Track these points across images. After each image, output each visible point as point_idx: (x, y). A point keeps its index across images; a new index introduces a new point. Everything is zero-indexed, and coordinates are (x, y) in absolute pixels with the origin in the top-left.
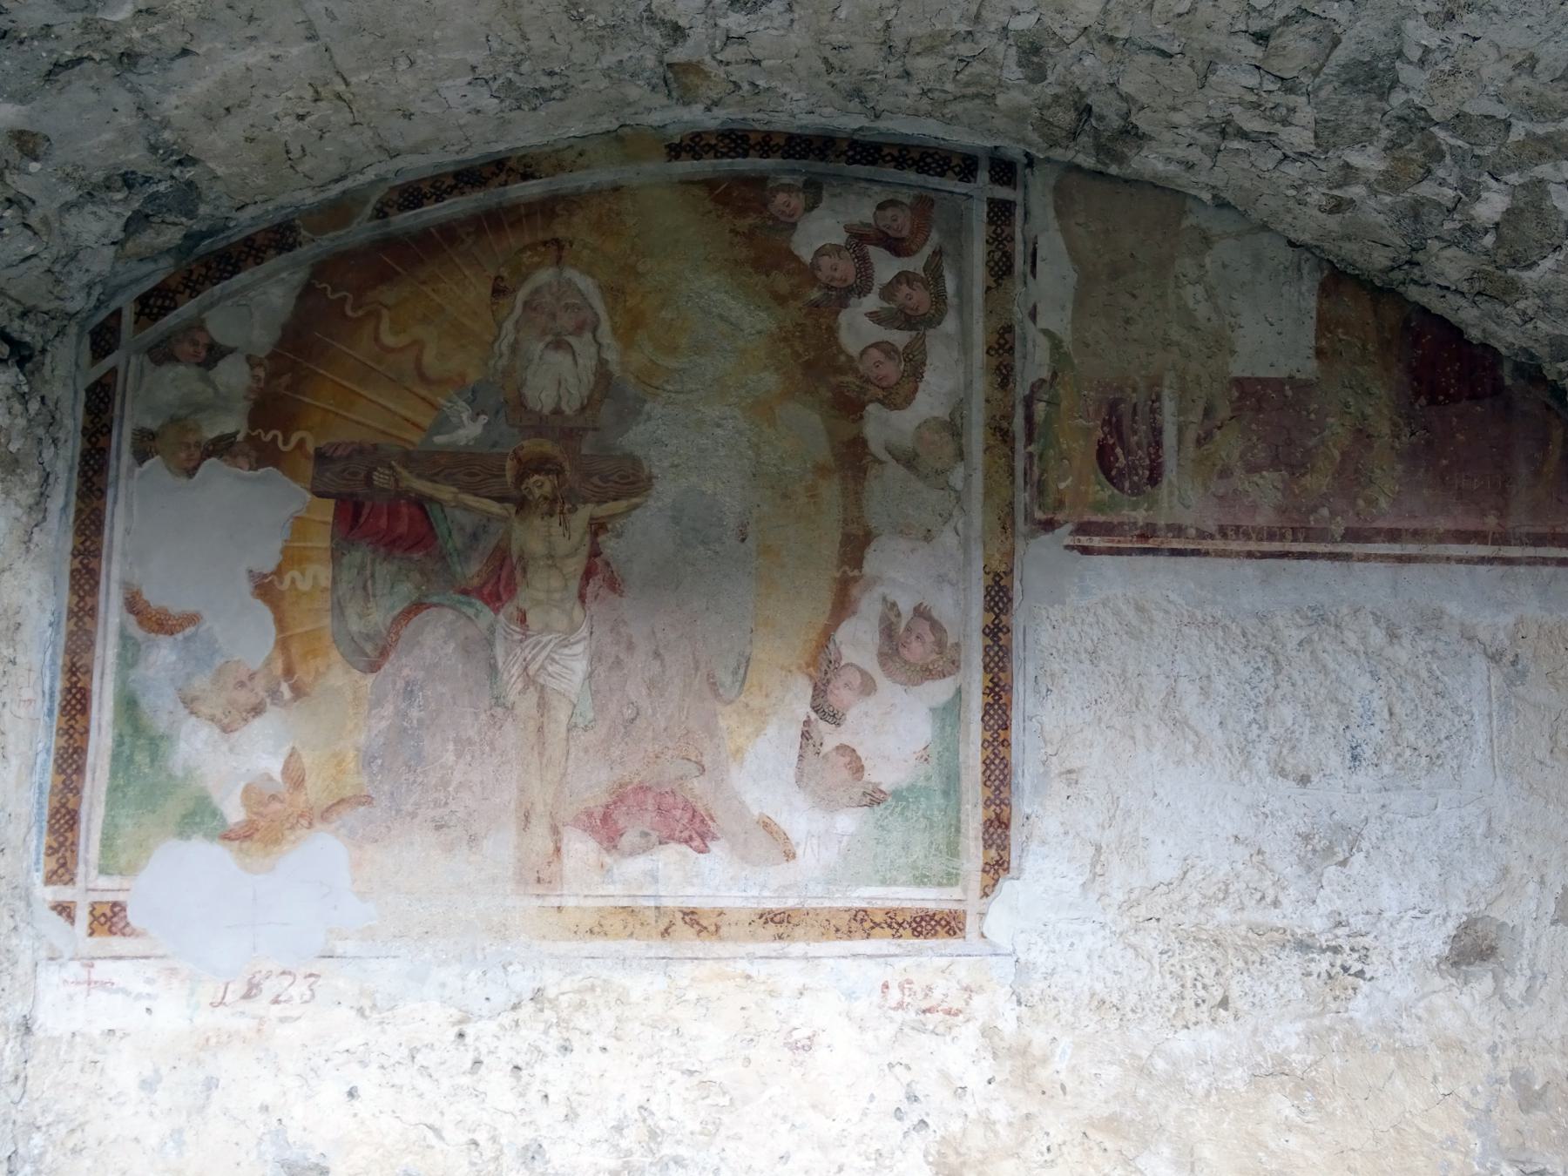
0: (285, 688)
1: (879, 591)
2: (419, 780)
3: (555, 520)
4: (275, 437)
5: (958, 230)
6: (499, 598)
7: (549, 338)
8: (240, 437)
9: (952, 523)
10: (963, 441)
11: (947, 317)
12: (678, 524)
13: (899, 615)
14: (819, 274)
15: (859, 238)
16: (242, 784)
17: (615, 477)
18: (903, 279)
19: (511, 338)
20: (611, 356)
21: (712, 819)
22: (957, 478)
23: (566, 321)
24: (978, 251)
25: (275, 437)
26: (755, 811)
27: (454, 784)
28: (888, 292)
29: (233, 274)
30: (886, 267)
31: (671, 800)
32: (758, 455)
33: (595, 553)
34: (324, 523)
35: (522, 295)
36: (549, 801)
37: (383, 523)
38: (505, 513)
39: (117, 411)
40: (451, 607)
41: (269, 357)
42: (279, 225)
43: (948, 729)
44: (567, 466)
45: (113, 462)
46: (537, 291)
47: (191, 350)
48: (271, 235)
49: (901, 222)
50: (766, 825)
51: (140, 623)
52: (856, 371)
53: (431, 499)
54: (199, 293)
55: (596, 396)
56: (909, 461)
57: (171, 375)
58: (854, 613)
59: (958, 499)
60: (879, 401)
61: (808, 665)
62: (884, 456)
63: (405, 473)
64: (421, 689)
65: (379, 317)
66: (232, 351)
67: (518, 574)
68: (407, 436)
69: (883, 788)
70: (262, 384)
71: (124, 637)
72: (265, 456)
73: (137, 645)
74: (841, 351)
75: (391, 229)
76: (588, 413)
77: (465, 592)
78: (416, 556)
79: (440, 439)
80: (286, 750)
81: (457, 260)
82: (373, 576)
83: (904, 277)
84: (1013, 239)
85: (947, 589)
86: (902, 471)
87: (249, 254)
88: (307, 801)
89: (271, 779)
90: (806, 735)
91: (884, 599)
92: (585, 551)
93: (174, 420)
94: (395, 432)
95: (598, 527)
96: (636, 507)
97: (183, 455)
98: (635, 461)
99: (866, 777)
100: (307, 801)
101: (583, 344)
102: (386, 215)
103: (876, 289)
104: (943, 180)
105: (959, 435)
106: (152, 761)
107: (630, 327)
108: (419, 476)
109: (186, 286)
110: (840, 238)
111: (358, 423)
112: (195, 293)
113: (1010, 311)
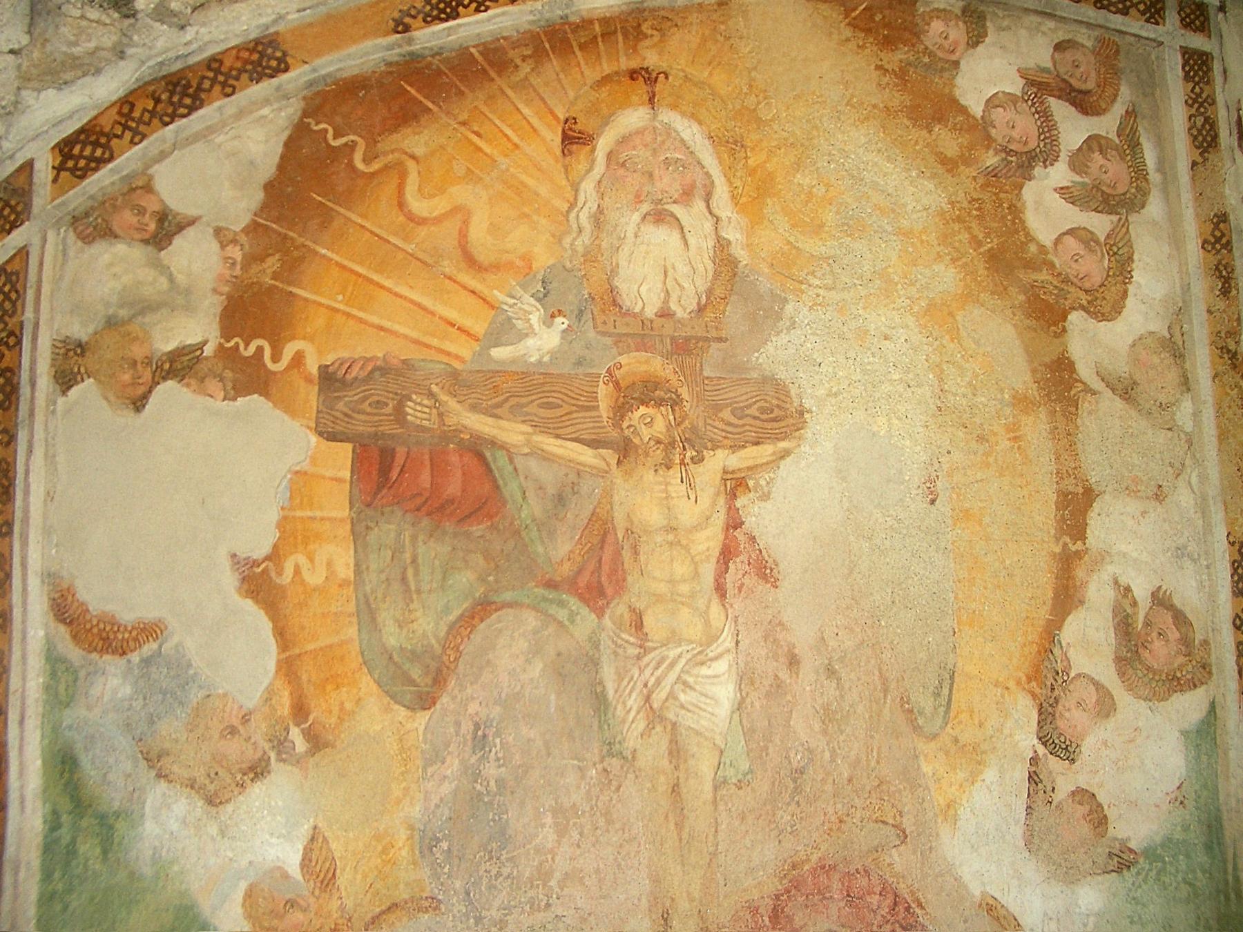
0: (295, 734)
1: (1110, 570)
2: (505, 871)
3: (675, 473)
4: (260, 350)
5: (1149, 84)
6: (602, 593)
7: (645, 207)
8: (209, 350)
9: (1184, 476)
10: (1187, 365)
11: (1151, 199)
12: (844, 479)
13: (1134, 604)
14: (993, 132)
15: (1039, 87)
16: (243, 886)
17: (753, 411)
18: (1095, 145)
19: (592, 206)
20: (732, 234)
21: (920, 905)
22: (1185, 409)
23: (668, 183)
24: (1177, 115)
25: (260, 350)
26: (976, 890)
27: (557, 875)
28: (1078, 162)
29: (192, 109)
30: (1074, 130)
31: (864, 882)
32: (941, 380)
33: (734, 523)
34: (340, 480)
35: (603, 144)
36: (696, 895)
37: (425, 478)
38: (603, 465)
39: (29, 314)
40: (535, 608)
41: (246, 231)
42: (257, 42)
43: (1204, 758)
44: (684, 393)
45: (25, 390)
46: (624, 140)
47: (134, 220)
48: (245, 55)
49: (1087, 76)
50: (990, 909)
51: (75, 637)
52: (1052, 265)
53: (493, 443)
54: (144, 137)
55: (719, 292)
56: (1127, 391)
57: (107, 258)
58: (1082, 602)
59: (1190, 443)
60: (1083, 308)
61: (1029, 680)
62: (1096, 384)
63: (452, 403)
64: (498, 734)
65: (403, 176)
66: (192, 222)
67: (626, 555)
68: (451, 348)
69: (1133, 845)
70: (238, 271)
71: (54, 660)
72: (249, 379)
73: (72, 670)
74: (1031, 239)
75: (416, 47)
76: (709, 315)
77: (551, 585)
78: (477, 529)
79: (500, 353)
80: (305, 829)
81: (509, 92)
82: (414, 561)
83: (1094, 143)
84: (1214, 103)
85: (1188, 564)
86: (1119, 403)
87: (214, 81)
88: (342, 908)
89: (286, 876)
90: (1033, 778)
91: (1116, 582)
92: (719, 520)
93: (111, 323)
94: (435, 342)
95: (735, 485)
96: (786, 454)
97: (127, 377)
98: (781, 389)
99: (1111, 831)
100: (342, 908)
101: (692, 215)
102: (407, 29)
103: (1064, 156)
104: (1127, 19)
105: (1182, 356)
106: (105, 852)
107: (756, 195)
108: (474, 408)
109: (126, 127)
110: (1015, 86)
111: (381, 328)
112: (139, 137)
113: (1222, 196)
